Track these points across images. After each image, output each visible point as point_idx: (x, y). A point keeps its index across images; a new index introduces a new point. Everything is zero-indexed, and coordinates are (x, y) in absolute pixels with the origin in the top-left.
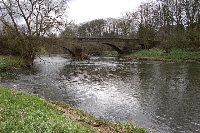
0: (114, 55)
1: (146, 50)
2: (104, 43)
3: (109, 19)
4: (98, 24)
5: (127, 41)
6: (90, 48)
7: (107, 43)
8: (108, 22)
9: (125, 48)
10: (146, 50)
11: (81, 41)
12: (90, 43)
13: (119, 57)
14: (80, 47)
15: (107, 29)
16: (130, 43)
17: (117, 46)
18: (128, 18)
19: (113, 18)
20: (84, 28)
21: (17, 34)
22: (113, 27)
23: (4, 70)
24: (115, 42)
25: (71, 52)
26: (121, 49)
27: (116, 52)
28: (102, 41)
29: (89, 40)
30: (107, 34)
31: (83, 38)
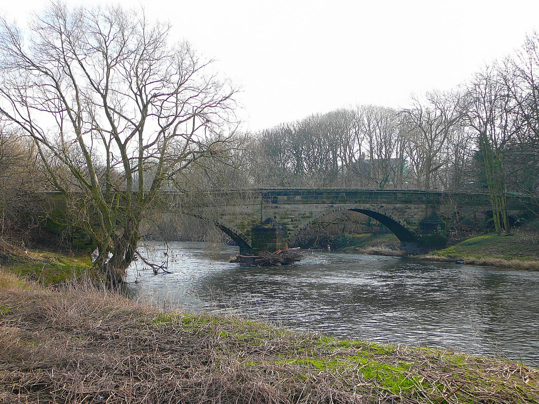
0: (387, 250)
1: (499, 234)
2: (351, 210)
3: (370, 111)
4: (324, 134)
5: (432, 199)
6: (302, 226)
7: (362, 206)
8: (366, 122)
9: (426, 225)
10: (499, 234)
11: (275, 202)
12: (304, 208)
13: (404, 259)
14: (268, 221)
15: (362, 148)
16: (442, 209)
17: (395, 218)
18: (438, 113)
19: (386, 107)
20: (273, 145)
21: (90, 187)
22: (386, 142)
23: (538, 270)
24: (389, 206)
25: (237, 240)
26: (412, 229)
27: (392, 237)
28: (345, 202)
29: (298, 198)
30: (361, 168)
31: (280, 194)
